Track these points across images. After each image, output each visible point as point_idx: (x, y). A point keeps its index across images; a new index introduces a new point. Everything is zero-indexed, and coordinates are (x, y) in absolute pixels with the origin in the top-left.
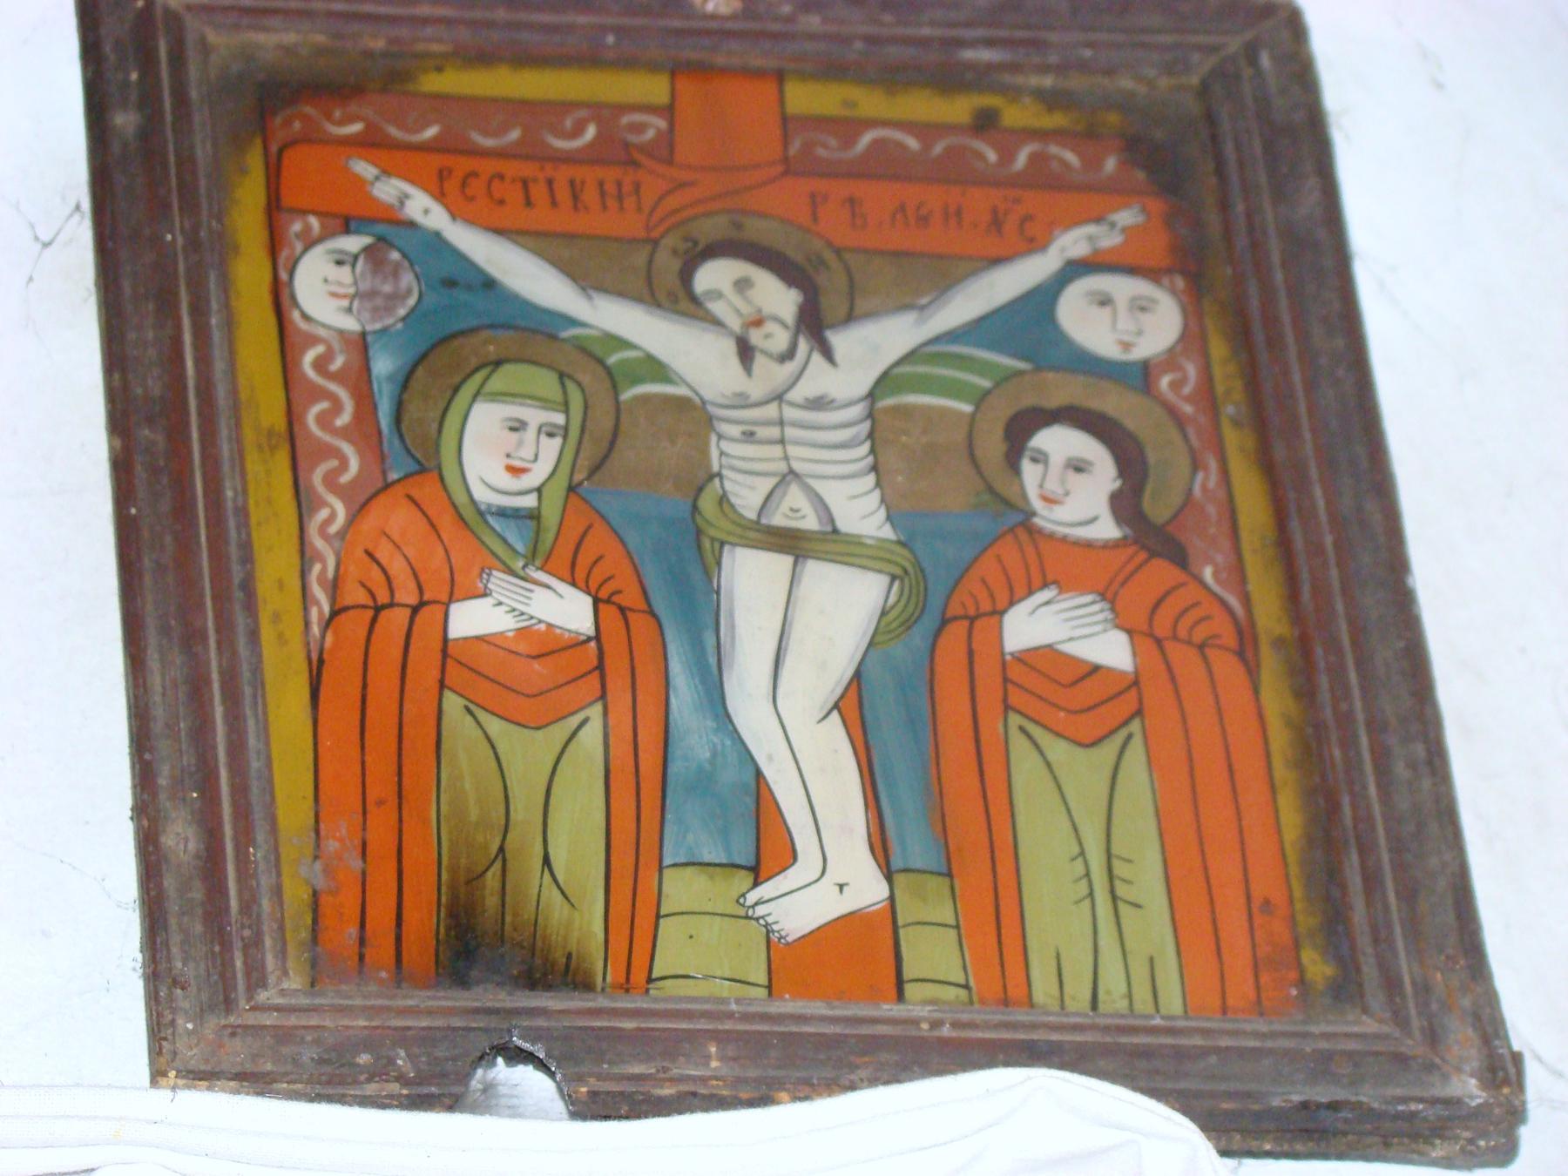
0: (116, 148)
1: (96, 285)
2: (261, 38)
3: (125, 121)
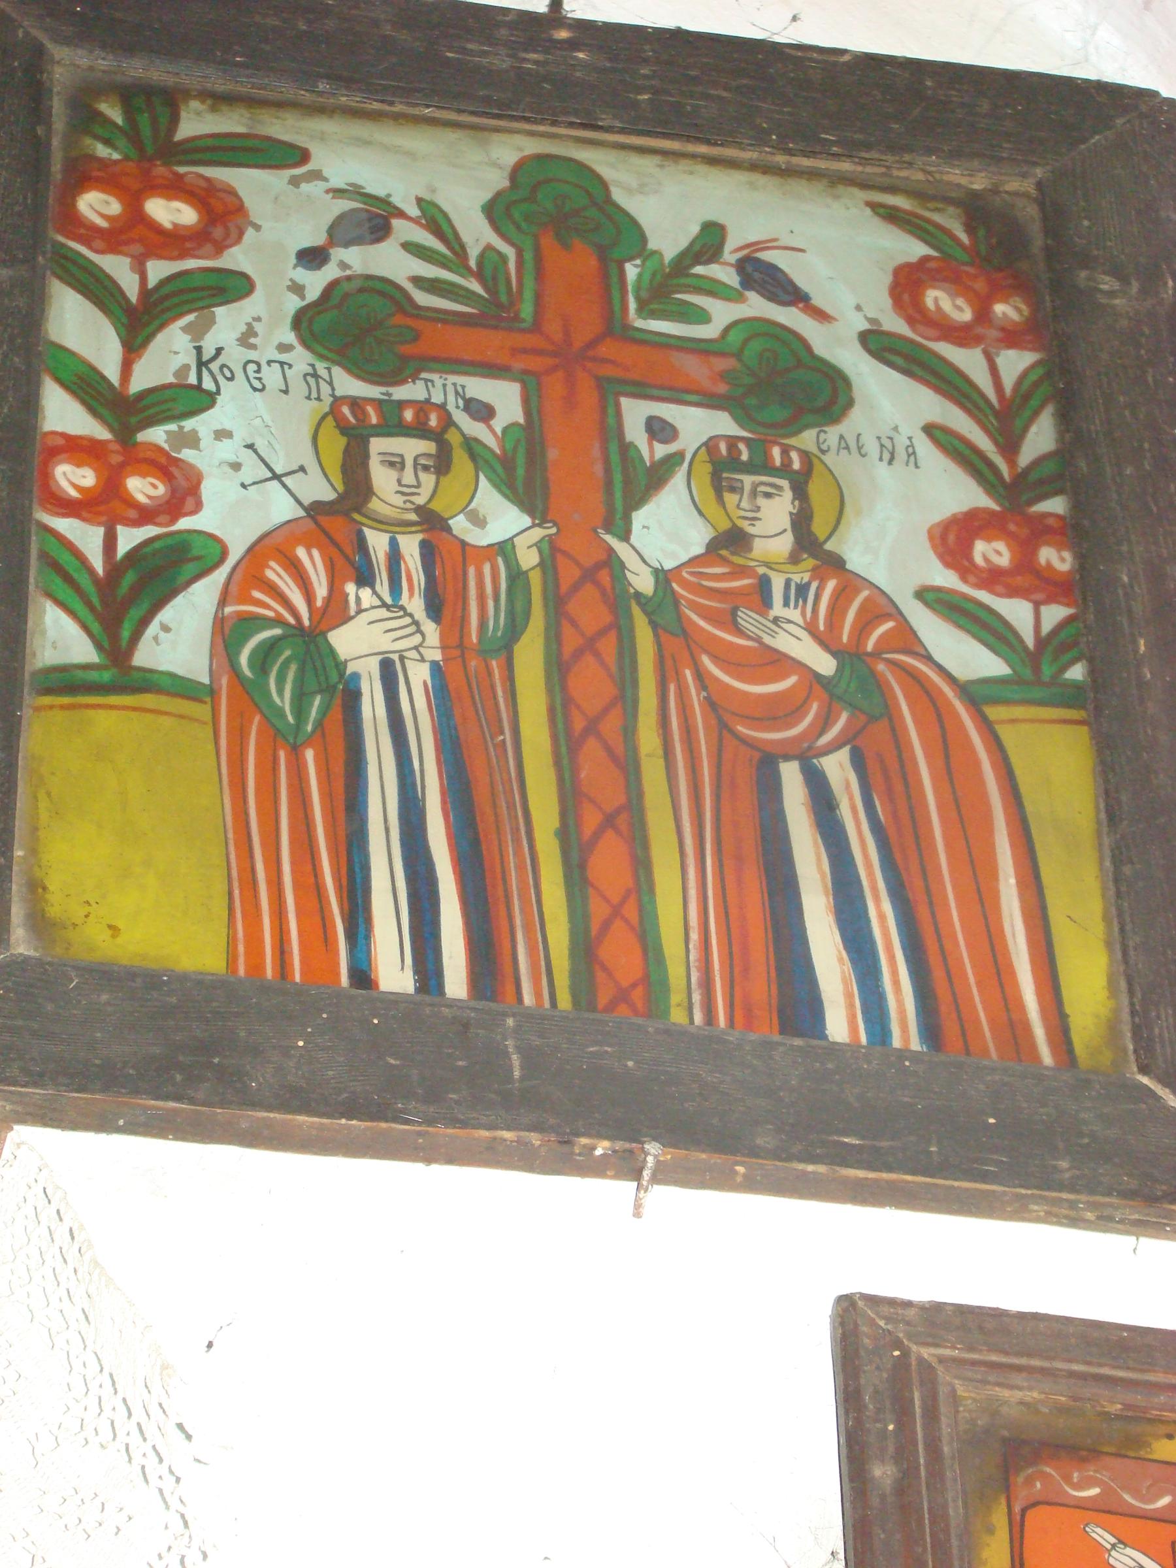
0: (875, 1501)
1: (437, 879)
2: (1005, 1393)
3: (883, 1472)
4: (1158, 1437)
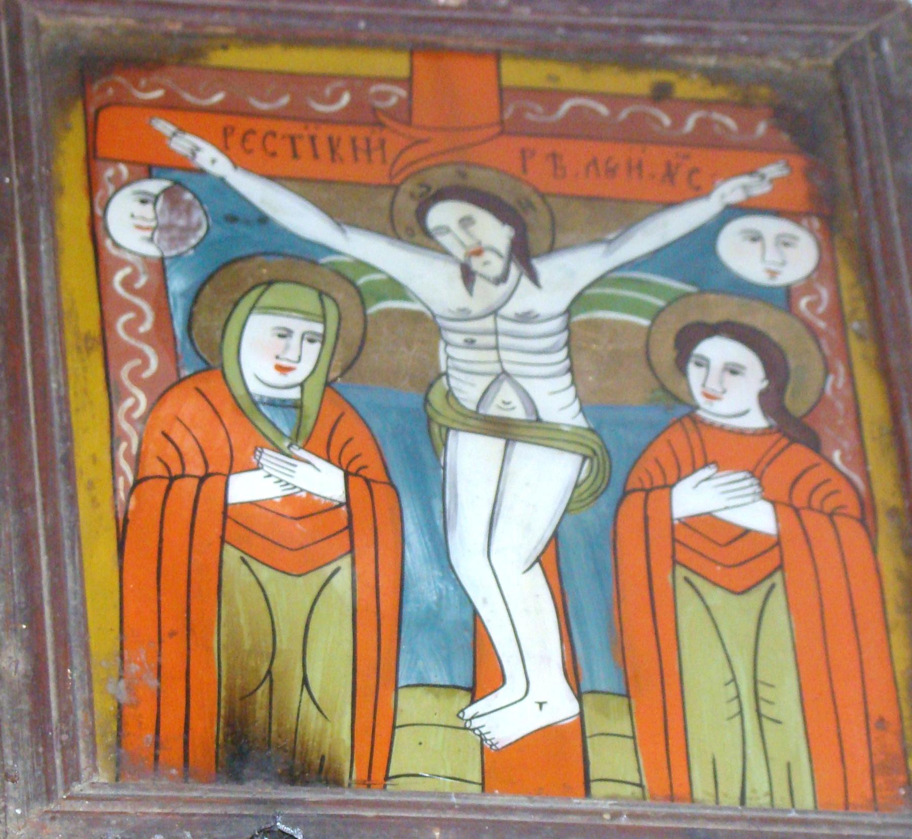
4: (214, 49)
